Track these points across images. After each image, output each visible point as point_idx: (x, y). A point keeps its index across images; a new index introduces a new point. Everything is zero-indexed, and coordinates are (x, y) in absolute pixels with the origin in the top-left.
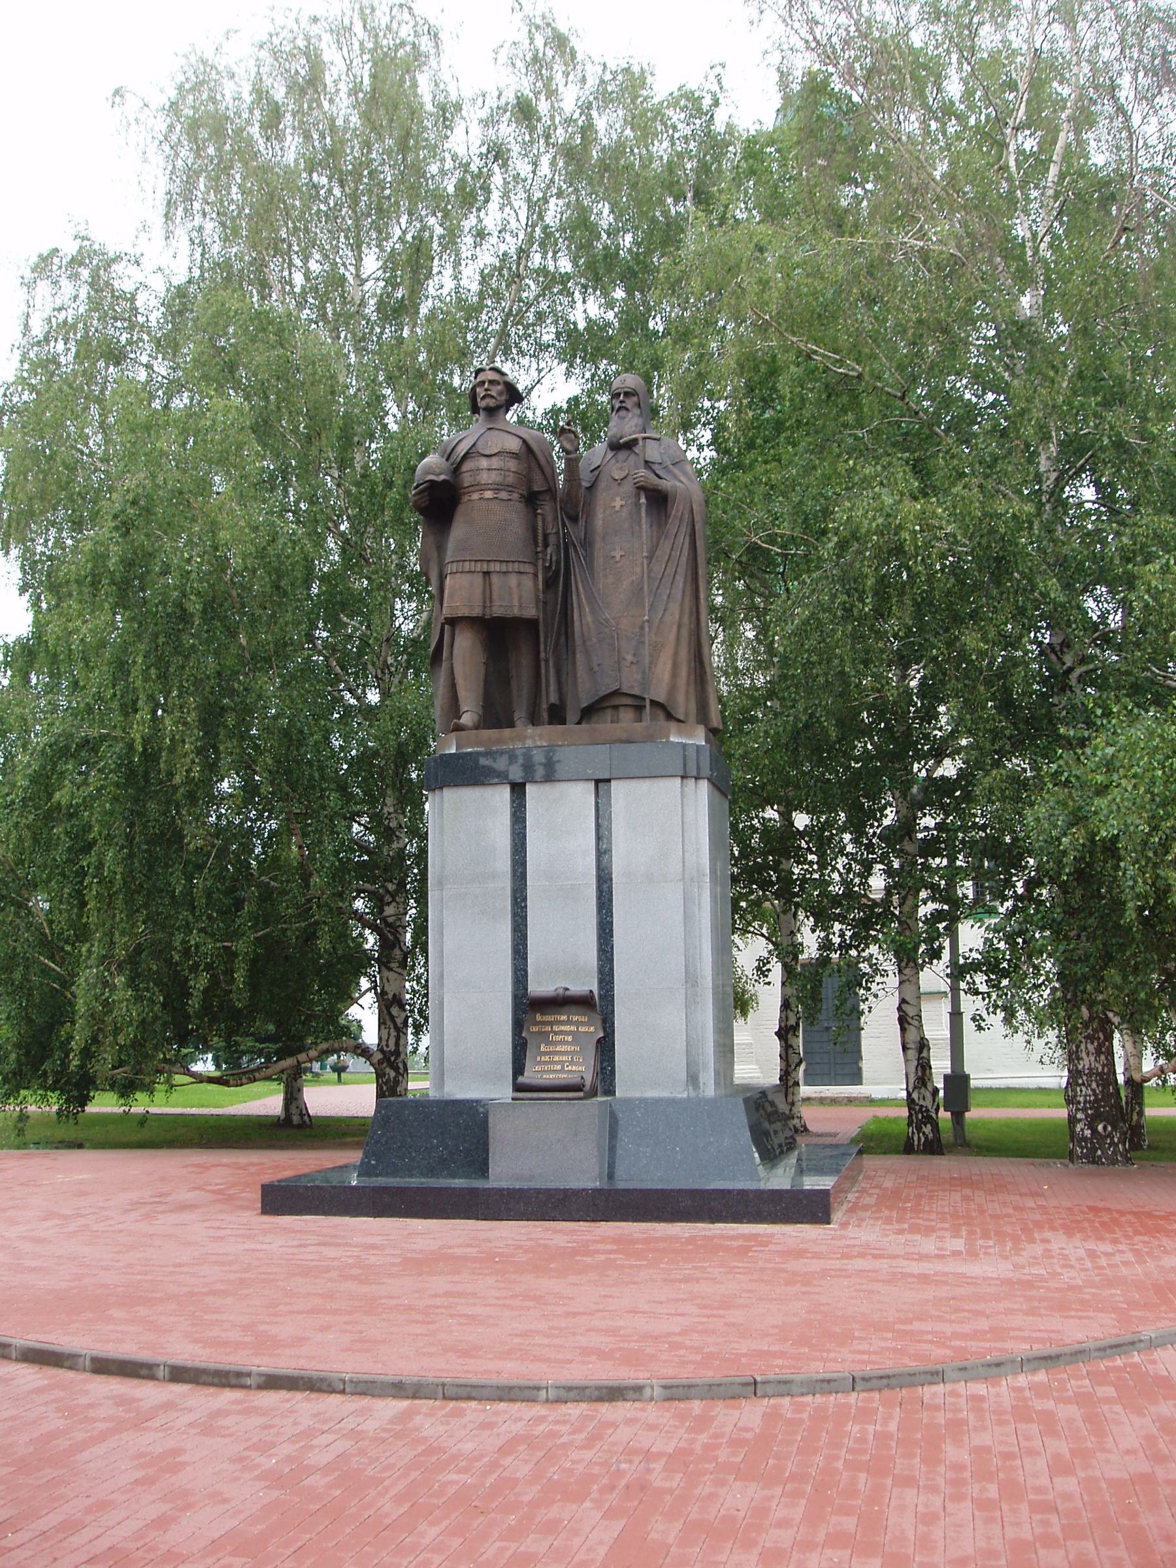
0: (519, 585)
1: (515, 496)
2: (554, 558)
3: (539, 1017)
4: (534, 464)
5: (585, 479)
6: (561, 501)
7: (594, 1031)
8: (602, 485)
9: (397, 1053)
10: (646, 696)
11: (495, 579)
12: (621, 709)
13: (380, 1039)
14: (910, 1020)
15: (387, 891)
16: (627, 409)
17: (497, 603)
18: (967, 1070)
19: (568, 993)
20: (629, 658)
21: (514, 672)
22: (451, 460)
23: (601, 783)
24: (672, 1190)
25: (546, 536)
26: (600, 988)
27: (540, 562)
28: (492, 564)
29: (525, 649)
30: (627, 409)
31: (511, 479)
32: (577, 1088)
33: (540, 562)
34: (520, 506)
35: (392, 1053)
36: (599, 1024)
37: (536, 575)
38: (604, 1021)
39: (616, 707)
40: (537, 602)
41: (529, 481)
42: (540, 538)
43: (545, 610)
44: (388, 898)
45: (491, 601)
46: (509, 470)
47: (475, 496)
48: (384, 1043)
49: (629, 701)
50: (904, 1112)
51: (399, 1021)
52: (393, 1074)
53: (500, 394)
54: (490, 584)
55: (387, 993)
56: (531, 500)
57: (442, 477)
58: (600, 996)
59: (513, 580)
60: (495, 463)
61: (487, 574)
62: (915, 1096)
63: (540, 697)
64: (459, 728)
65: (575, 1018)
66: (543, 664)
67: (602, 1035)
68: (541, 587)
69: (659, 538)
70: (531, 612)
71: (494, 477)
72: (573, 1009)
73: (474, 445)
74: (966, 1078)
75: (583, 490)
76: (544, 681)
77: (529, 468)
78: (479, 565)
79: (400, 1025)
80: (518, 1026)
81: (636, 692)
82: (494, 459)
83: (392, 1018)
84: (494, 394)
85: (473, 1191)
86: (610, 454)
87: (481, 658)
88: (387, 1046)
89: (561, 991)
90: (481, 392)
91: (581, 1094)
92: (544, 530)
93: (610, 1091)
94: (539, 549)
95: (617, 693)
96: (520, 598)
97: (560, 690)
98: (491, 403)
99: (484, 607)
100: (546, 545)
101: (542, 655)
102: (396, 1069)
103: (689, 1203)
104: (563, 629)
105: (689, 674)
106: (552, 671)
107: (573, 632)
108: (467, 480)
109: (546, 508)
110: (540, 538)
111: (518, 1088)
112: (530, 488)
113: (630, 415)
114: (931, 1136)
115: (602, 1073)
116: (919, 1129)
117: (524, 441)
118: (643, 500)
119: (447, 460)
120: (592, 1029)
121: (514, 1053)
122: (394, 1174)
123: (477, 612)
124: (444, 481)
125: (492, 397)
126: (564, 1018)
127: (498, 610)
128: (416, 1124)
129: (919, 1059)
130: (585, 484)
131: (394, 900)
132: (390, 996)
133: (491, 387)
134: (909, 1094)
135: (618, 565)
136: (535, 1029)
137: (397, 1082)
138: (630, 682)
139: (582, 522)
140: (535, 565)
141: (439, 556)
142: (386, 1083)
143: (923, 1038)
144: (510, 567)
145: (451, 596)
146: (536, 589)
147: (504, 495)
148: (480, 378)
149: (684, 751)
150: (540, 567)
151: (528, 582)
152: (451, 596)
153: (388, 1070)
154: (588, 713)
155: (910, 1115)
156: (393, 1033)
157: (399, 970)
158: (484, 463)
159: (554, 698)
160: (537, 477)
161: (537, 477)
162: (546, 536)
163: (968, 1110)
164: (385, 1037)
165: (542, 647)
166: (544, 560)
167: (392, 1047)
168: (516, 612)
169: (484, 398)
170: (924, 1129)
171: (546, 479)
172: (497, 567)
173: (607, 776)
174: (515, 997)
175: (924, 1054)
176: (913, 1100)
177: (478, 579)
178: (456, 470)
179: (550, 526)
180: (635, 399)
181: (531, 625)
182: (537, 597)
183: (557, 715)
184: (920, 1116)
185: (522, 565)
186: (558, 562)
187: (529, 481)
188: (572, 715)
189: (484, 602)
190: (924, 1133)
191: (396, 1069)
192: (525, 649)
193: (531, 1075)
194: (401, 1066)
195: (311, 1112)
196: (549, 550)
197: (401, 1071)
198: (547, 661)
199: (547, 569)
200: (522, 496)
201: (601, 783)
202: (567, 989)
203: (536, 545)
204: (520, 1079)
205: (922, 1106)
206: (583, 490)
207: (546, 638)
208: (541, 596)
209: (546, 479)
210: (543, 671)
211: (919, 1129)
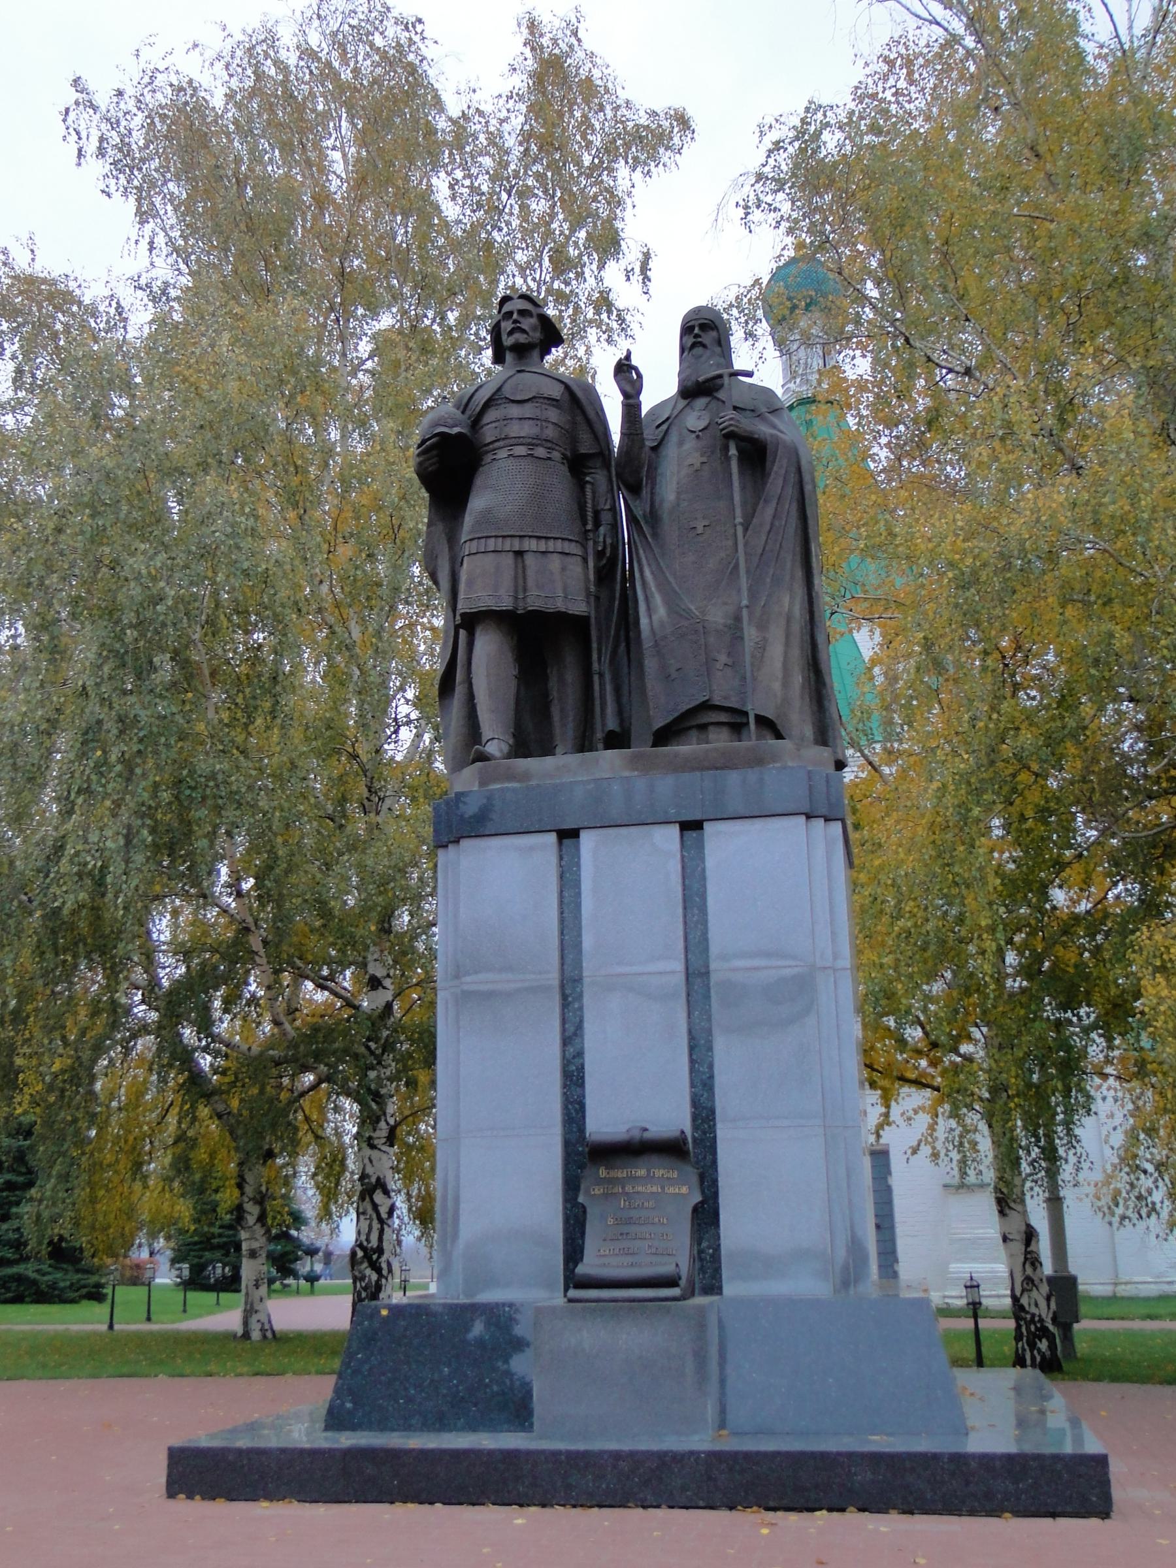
0: (563, 569)
1: (556, 455)
2: (609, 541)
3: (603, 1172)
4: (579, 418)
5: (650, 436)
6: (617, 465)
7: (690, 1194)
8: (673, 438)
9: (380, 1250)
10: (748, 708)
11: (529, 560)
12: (711, 728)
13: (359, 1233)
14: (1012, 1205)
15: (372, 1053)
16: (704, 346)
17: (533, 592)
18: (1073, 1269)
19: (647, 1135)
20: (723, 658)
21: (554, 694)
22: (468, 412)
23: (691, 826)
24: (839, 1454)
25: (597, 514)
26: (695, 1128)
27: (591, 543)
28: (526, 542)
29: (570, 659)
30: (704, 346)
31: (550, 432)
32: (670, 1282)
33: (591, 543)
34: (564, 469)
35: (374, 1251)
36: (695, 1180)
37: (585, 560)
38: (702, 1178)
39: (703, 727)
40: (588, 594)
41: (574, 441)
42: (590, 514)
43: (597, 608)
44: (372, 1060)
45: (525, 590)
46: (546, 421)
47: (503, 454)
48: (363, 1238)
49: (723, 717)
50: (1011, 1324)
51: (383, 1211)
52: (374, 1277)
53: (534, 328)
54: (524, 568)
55: (368, 1176)
56: (578, 465)
57: (456, 430)
58: (695, 1139)
59: (555, 562)
60: (528, 410)
61: (519, 554)
62: (1024, 1301)
63: (593, 717)
64: (482, 757)
65: (659, 1173)
66: (596, 678)
67: (698, 1198)
68: (592, 577)
69: (756, 505)
70: (579, 607)
71: (527, 430)
72: (655, 1159)
73: (499, 389)
74: (1072, 1281)
75: (647, 449)
76: (597, 702)
77: (574, 423)
78: (508, 541)
79: (384, 1216)
80: (571, 1186)
81: (733, 703)
82: (528, 406)
83: (375, 1207)
84: (524, 326)
85: (511, 1456)
86: (682, 403)
87: (510, 669)
88: (368, 1240)
89: (636, 1134)
90: (507, 326)
91: (675, 1292)
92: (594, 506)
93: (713, 1287)
94: (589, 527)
95: (706, 706)
96: (565, 589)
97: (620, 712)
98: (520, 338)
99: (516, 598)
100: (597, 524)
101: (595, 666)
102: (378, 1270)
103: (869, 1476)
104: (622, 633)
105: (803, 687)
106: (609, 688)
107: (639, 632)
108: (489, 434)
109: (598, 478)
110: (590, 514)
111: (573, 1281)
112: (574, 450)
113: (708, 353)
114: (1048, 1353)
115: (701, 1260)
116: (1032, 1346)
117: (567, 387)
118: (733, 451)
119: (463, 412)
120: (684, 1190)
121: (566, 1230)
122: (382, 1425)
123: (506, 604)
124: (460, 434)
125: (523, 331)
126: (642, 1172)
127: (535, 601)
128: (416, 1342)
129: (1026, 1253)
130: (649, 444)
131: (379, 1063)
132: (373, 1180)
133: (521, 319)
134: (1015, 1299)
135: (701, 539)
136: (598, 1191)
137: (379, 1287)
138: (722, 691)
139: (645, 493)
140: (584, 547)
141: (451, 548)
142: (365, 1289)
143: (1029, 1226)
144: (551, 545)
145: (470, 583)
146: (587, 580)
147: (541, 452)
148: (507, 307)
149: (810, 778)
150: (590, 551)
151: (575, 568)
152: (470, 583)
153: (368, 1272)
154: (663, 737)
155: (1018, 1327)
156: (376, 1225)
157: (384, 1148)
158: (515, 411)
159: (612, 724)
160: (585, 437)
161: (585, 437)
162: (597, 514)
163: (1077, 1322)
164: (365, 1229)
165: (595, 656)
166: (596, 543)
167: (374, 1243)
168: (560, 605)
169: (511, 333)
170: (1039, 1345)
171: (596, 438)
172: (533, 545)
173: (698, 817)
174: (567, 1144)
175: (1032, 1248)
176: (1022, 1308)
177: (509, 560)
178: (476, 423)
179: (602, 500)
180: (714, 334)
181: (576, 626)
182: (587, 589)
183: (617, 740)
184: (1033, 1328)
185: (566, 543)
186: (614, 547)
187: (574, 441)
188: (641, 732)
189: (516, 591)
190: (1039, 1351)
191: (378, 1270)
192: (570, 659)
193: (587, 1267)
194: (384, 1266)
195: (276, 1327)
196: (602, 530)
197: (385, 1272)
198: (601, 675)
199: (600, 555)
200: (565, 457)
201: (691, 826)
202: (646, 1130)
203: (585, 523)
204: (581, 1269)
205: (1033, 1315)
206: (647, 449)
207: (599, 644)
208: (593, 588)
209: (596, 438)
210: (597, 687)
211: (1032, 1346)
